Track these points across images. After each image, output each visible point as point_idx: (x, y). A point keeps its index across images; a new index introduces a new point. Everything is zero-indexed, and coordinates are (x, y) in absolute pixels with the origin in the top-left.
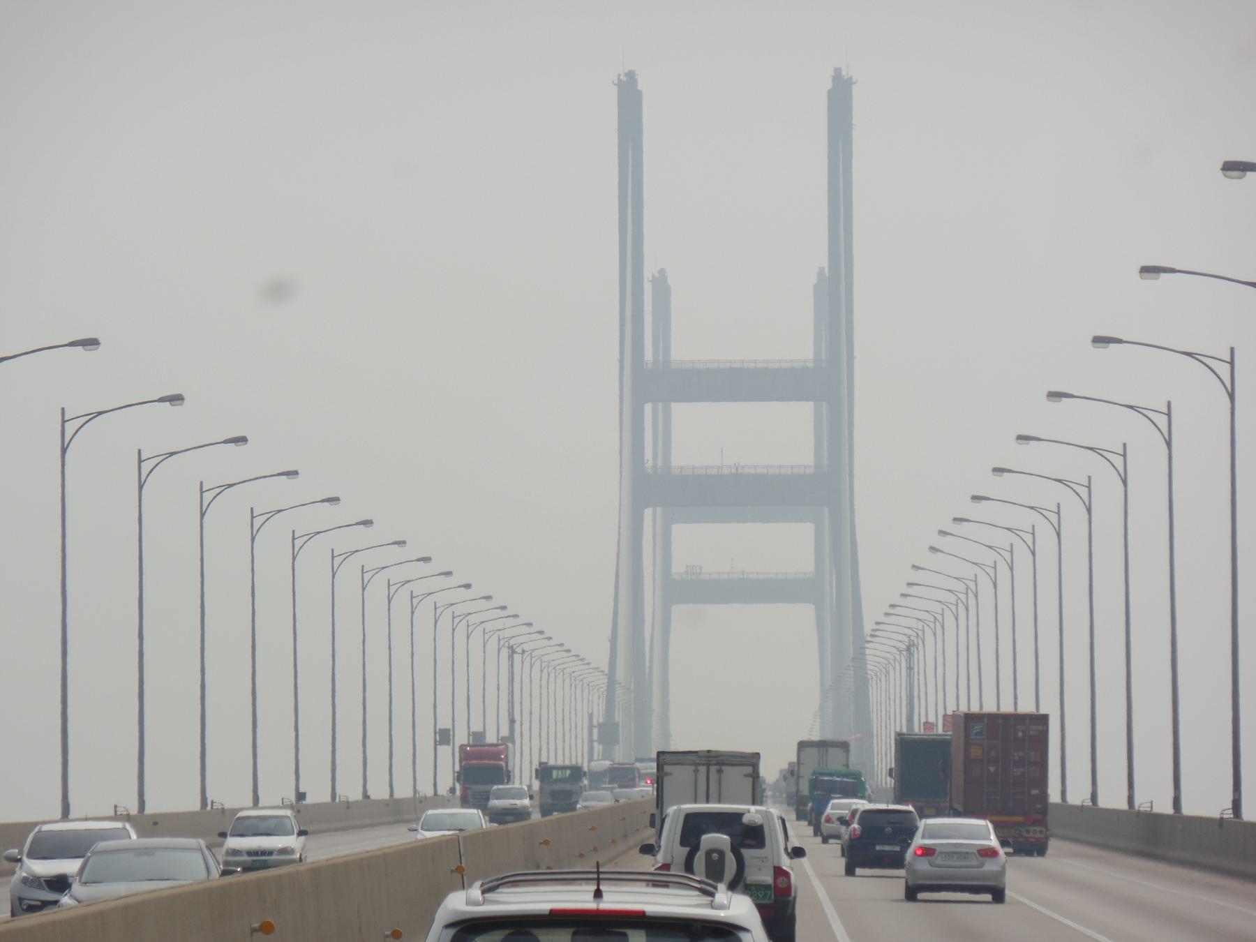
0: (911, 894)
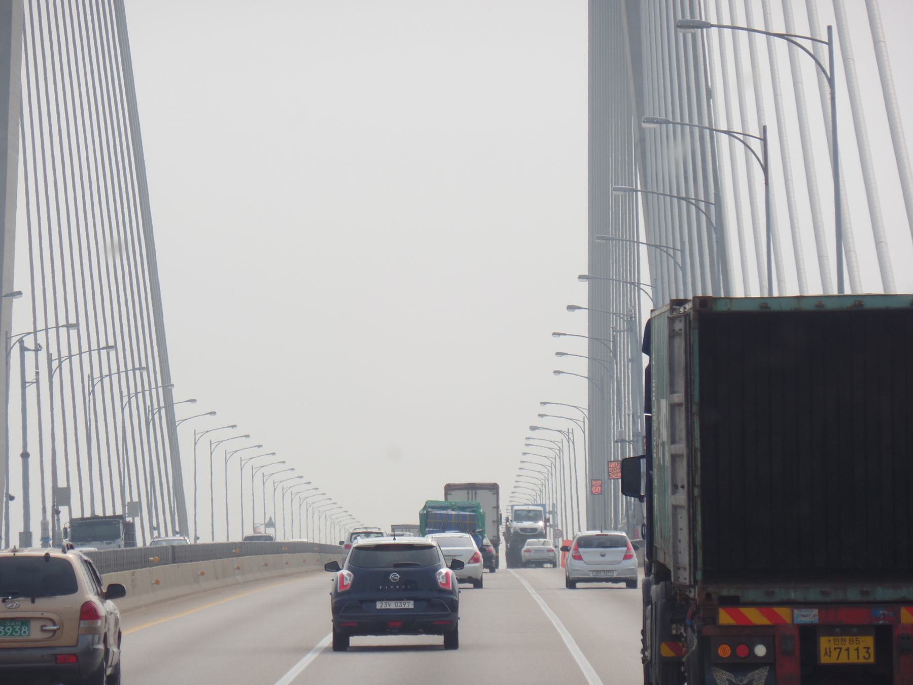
0: (571, 584)
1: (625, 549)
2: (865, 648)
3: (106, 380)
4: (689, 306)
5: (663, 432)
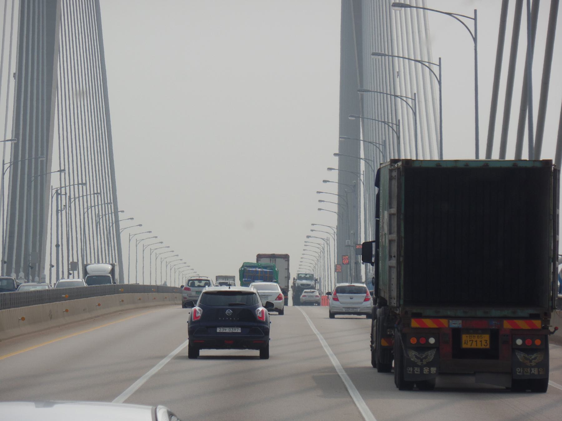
0: (332, 315)
1: (365, 295)
2: (485, 340)
4: (400, 164)
5: (385, 228)
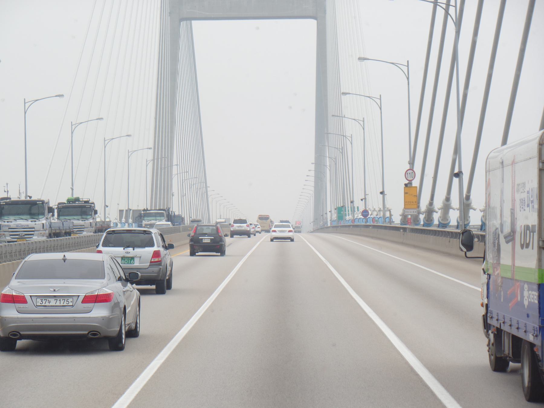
3: (194, 185)
